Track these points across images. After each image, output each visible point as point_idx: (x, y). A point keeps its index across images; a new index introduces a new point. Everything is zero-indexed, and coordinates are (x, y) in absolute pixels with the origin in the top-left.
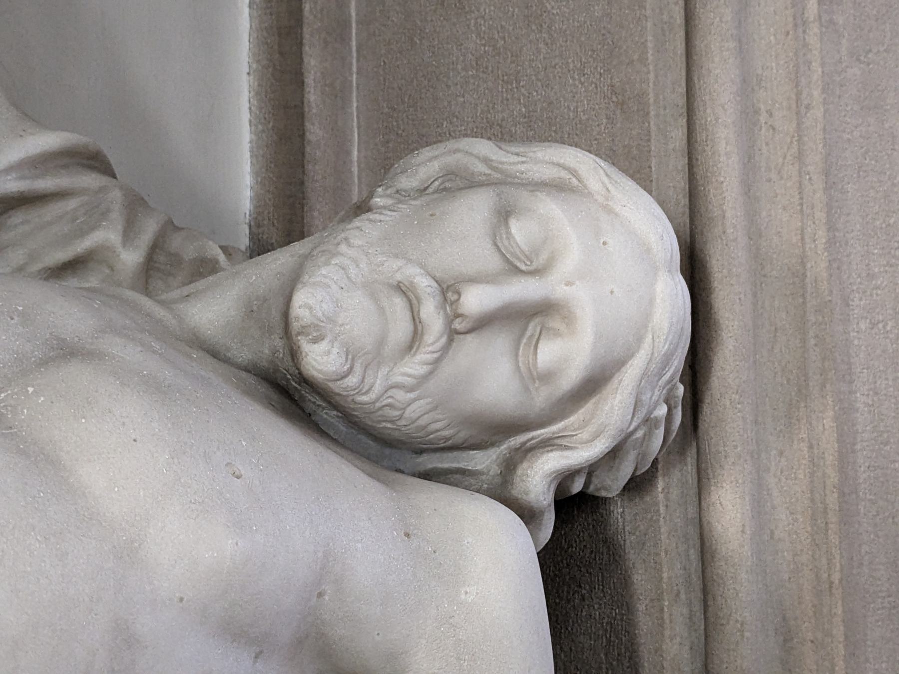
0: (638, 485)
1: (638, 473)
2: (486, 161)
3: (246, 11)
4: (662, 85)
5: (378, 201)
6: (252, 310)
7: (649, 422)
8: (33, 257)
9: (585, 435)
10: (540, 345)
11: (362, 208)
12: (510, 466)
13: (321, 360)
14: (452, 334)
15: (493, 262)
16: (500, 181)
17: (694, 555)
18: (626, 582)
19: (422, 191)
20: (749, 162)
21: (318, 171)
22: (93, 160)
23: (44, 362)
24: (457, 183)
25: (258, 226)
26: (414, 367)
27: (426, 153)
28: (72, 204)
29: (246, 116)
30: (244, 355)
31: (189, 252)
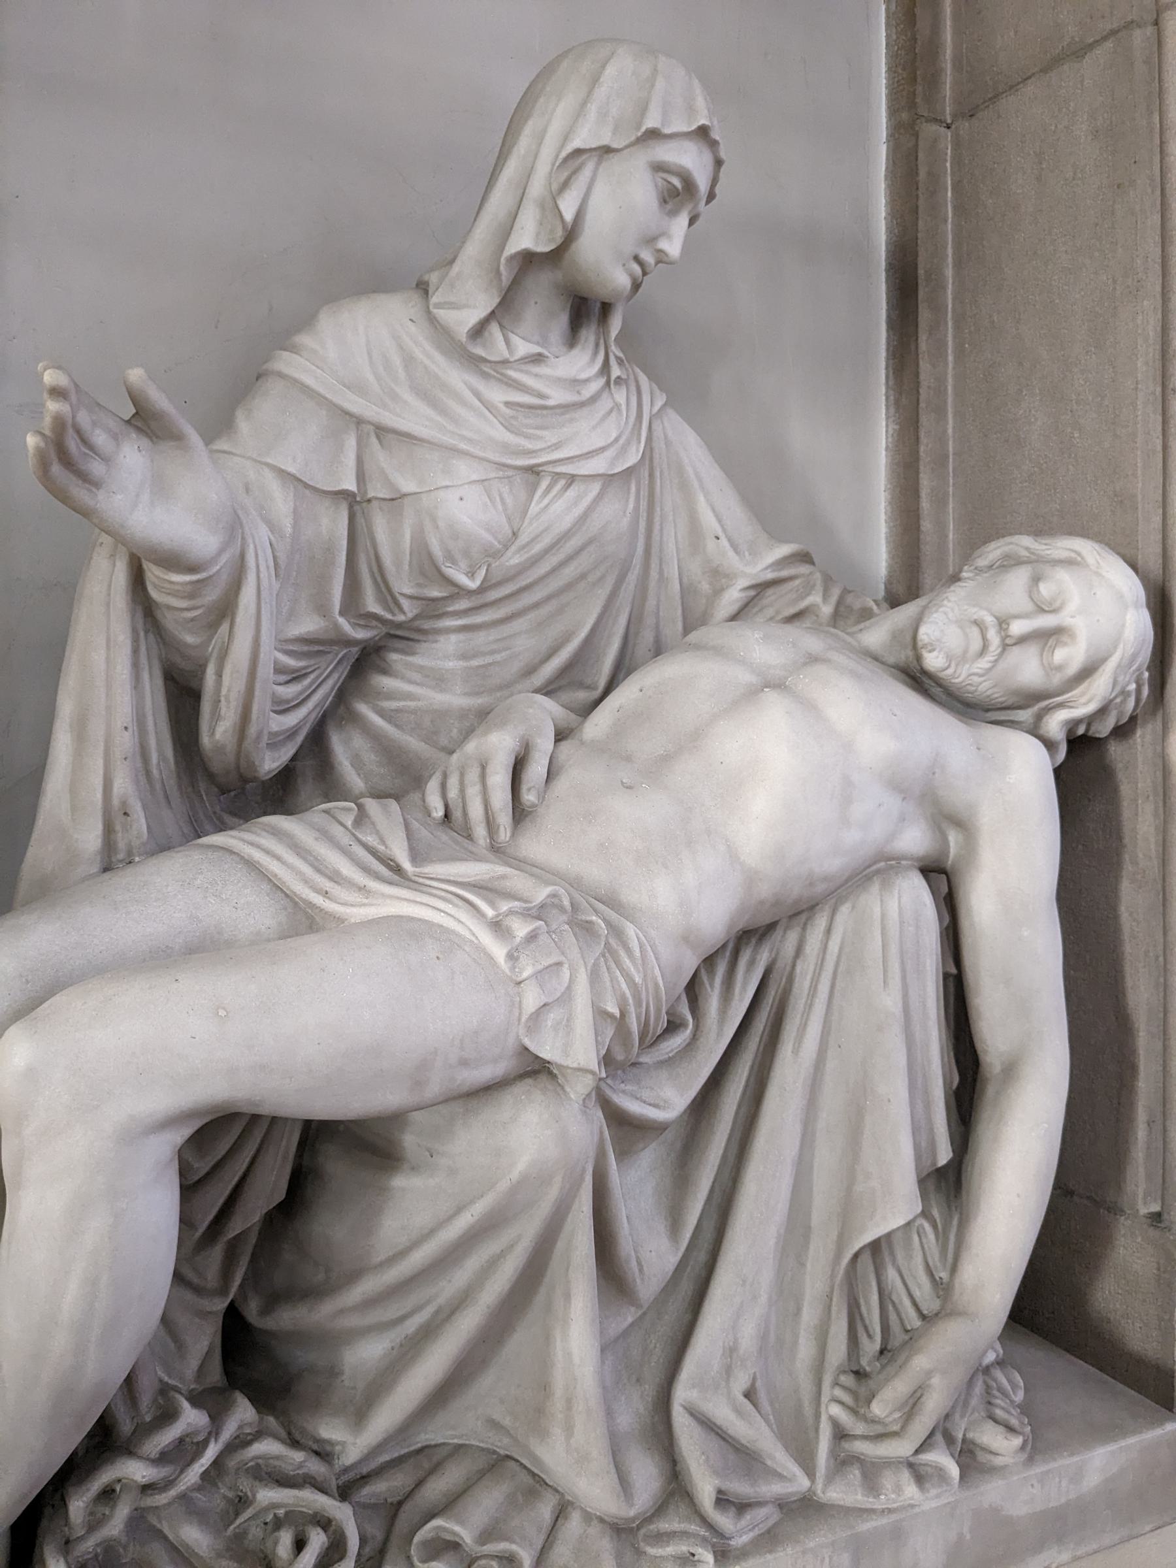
0: (1123, 731)
1: (1121, 723)
2: (1027, 549)
3: (884, 453)
4: (1145, 488)
5: (964, 574)
6: (896, 636)
7: (1124, 693)
8: (778, 612)
9: (1083, 700)
11: (955, 578)
12: (1039, 717)
13: (933, 661)
14: (1005, 646)
15: (1030, 607)
16: (1035, 560)
17: (1159, 774)
18: (1116, 790)
19: (990, 567)
21: (928, 549)
22: (804, 558)
23: (805, 664)
24: (1010, 562)
25: (891, 584)
26: (983, 664)
27: (993, 545)
28: (797, 582)
29: (883, 517)
30: (891, 660)
31: (857, 605)
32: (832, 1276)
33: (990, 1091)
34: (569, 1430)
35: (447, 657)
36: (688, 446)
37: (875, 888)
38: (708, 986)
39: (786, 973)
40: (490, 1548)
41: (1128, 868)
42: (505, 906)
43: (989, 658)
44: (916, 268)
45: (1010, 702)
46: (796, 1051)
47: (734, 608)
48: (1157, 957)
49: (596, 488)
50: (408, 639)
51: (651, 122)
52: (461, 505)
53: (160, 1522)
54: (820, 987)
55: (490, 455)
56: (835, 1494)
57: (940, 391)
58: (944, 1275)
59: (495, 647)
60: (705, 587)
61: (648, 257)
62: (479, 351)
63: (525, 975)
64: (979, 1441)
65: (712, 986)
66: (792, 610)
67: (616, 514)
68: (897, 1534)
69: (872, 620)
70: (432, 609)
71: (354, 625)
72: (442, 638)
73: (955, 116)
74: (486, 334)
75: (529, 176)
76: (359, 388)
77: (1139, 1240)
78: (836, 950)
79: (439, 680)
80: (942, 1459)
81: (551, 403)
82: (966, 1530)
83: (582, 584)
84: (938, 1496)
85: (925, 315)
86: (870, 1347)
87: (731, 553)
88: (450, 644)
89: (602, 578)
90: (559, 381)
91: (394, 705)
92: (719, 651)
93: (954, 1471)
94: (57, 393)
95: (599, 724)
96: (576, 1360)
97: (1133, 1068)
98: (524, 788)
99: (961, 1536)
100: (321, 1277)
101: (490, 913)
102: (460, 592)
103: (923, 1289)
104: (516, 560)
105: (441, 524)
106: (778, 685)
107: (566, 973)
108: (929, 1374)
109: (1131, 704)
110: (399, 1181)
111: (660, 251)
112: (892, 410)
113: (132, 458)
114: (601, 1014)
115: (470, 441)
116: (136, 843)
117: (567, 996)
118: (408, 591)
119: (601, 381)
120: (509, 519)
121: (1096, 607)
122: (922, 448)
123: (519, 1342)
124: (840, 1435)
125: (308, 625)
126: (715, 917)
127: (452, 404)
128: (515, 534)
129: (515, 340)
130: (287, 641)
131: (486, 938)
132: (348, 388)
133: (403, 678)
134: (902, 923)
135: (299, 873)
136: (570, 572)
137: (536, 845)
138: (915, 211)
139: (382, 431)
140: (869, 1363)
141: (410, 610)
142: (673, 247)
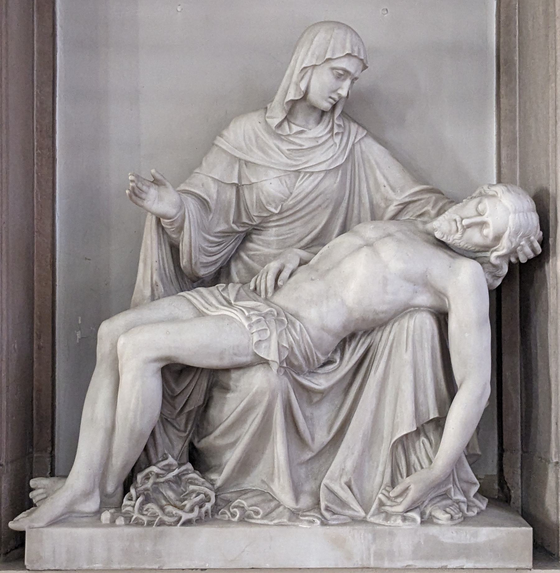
8: (414, 213)
10: (534, 219)
15: (475, 213)
26: (458, 235)
28: (422, 201)
34: (279, 478)
35: (271, 236)
36: (373, 150)
37: (407, 318)
46: (375, 373)
51: (328, 57)
52: (270, 186)
55: (282, 168)
57: (513, 111)
59: (288, 232)
60: (383, 205)
62: (280, 132)
66: (419, 213)
68: (391, 534)
70: (265, 219)
71: (238, 227)
72: (270, 230)
74: (283, 126)
76: (240, 149)
79: (268, 244)
80: (415, 515)
81: (304, 148)
83: (320, 209)
84: (409, 525)
87: (390, 192)
88: (273, 231)
89: (327, 207)
90: (306, 139)
91: (252, 253)
93: (419, 519)
94: (132, 181)
101: (247, 314)
102: (273, 214)
104: (291, 203)
105: (265, 193)
107: (268, 332)
110: (229, 396)
111: (339, 94)
113: (153, 192)
115: (275, 164)
116: (161, 294)
117: (269, 339)
118: (256, 214)
120: (289, 189)
125: (223, 227)
127: (270, 152)
128: (291, 193)
129: (293, 126)
130: (215, 233)
132: (236, 149)
136: (314, 205)
137: (280, 299)
139: (247, 163)
141: (257, 221)
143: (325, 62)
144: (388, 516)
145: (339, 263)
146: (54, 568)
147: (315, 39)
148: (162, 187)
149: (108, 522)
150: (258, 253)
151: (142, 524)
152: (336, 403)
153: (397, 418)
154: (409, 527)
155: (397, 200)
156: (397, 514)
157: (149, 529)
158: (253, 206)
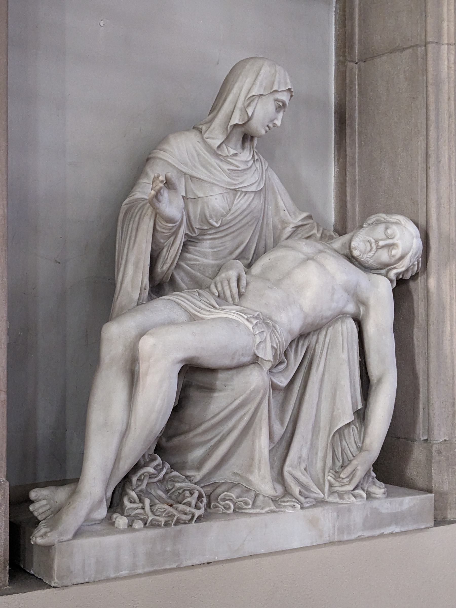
0: (414, 277)
2: (384, 218)
5: (364, 226)
6: (343, 245)
7: (413, 265)
8: (303, 235)
9: (401, 267)
11: (361, 227)
13: (356, 253)
14: (377, 249)
15: (385, 237)
16: (386, 222)
17: (426, 292)
18: (412, 298)
19: (372, 224)
20: (439, 215)
21: (349, 214)
24: (378, 223)
26: (371, 254)
27: (373, 216)
28: (309, 226)
30: (342, 253)
31: (328, 234)
32: (327, 442)
33: (373, 388)
34: (259, 470)
35: (206, 248)
38: (290, 350)
39: (313, 349)
40: (240, 499)
41: (416, 324)
42: (249, 316)
43: (372, 252)
44: (345, 114)
45: (378, 267)
46: (317, 371)
47: (288, 234)
48: (426, 353)
49: (252, 195)
50: (193, 242)
51: (275, 88)
53: (151, 489)
54: (324, 352)
56: (331, 499)
57: (354, 158)
58: (360, 445)
59: (220, 245)
60: (280, 226)
61: (271, 125)
62: (220, 153)
63: (257, 333)
64: (371, 491)
65: (291, 352)
66: (307, 235)
67: (257, 203)
68: (349, 510)
69: (334, 240)
70: (203, 232)
72: (205, 242)
73: (359, 61)
75: (237, 101)
76: (186, 164)
77: (421, 448)
78: (328, 341)
79: (205, 255)
81: (240, 169)
82: (368, 513)
83: (247, 226)
85: (348, 131)
86: (339, 464)
88: (207, 243)
91: (192, 263)
92: (292, 248)
93: (365, 496)
95: (256, 269)
96: (263, 447)
97: (419, 391)
98: (241, 287)
99: (367, 515)
100: (188, 427)
101: (246, 317)
103: (354, 449)
104: (230, 218)
106: (312, 259)
107: (265, 333)
108: (357, 465)
109: (416, 268)
110: (216, 395)
112: (336, 163)
114: (273, 347)
115: (219, 181)
118: (198, 227)
119: (253, 160)
121: (405, 238)
122: (347, 179)
123: (246, 444)
124: (331, 486)
126: (297, 326)
127: (213, 170)
128: (230, 210)
131: (247, 323)
133: (193, 254)
134: (347, 333)
135: (191, 306)
136: (244, 222)
138: (345, 94)
139: (192, 177)
140: (339, 469)
142: (278, 123)
143: (271, 93)
144: (341, 495)
145: (288, 274)
146: (83, 582)
147: (262, 71)
148: (172, 191)
149: (126, 527)
150: (198, 262)
151: (159, 526)
152: (278, 399)
153: (338, 409)
154: (360, 503)
155: (293, 223)
156: (347, 492)
157: (169, 529)
158: (195, 219)
